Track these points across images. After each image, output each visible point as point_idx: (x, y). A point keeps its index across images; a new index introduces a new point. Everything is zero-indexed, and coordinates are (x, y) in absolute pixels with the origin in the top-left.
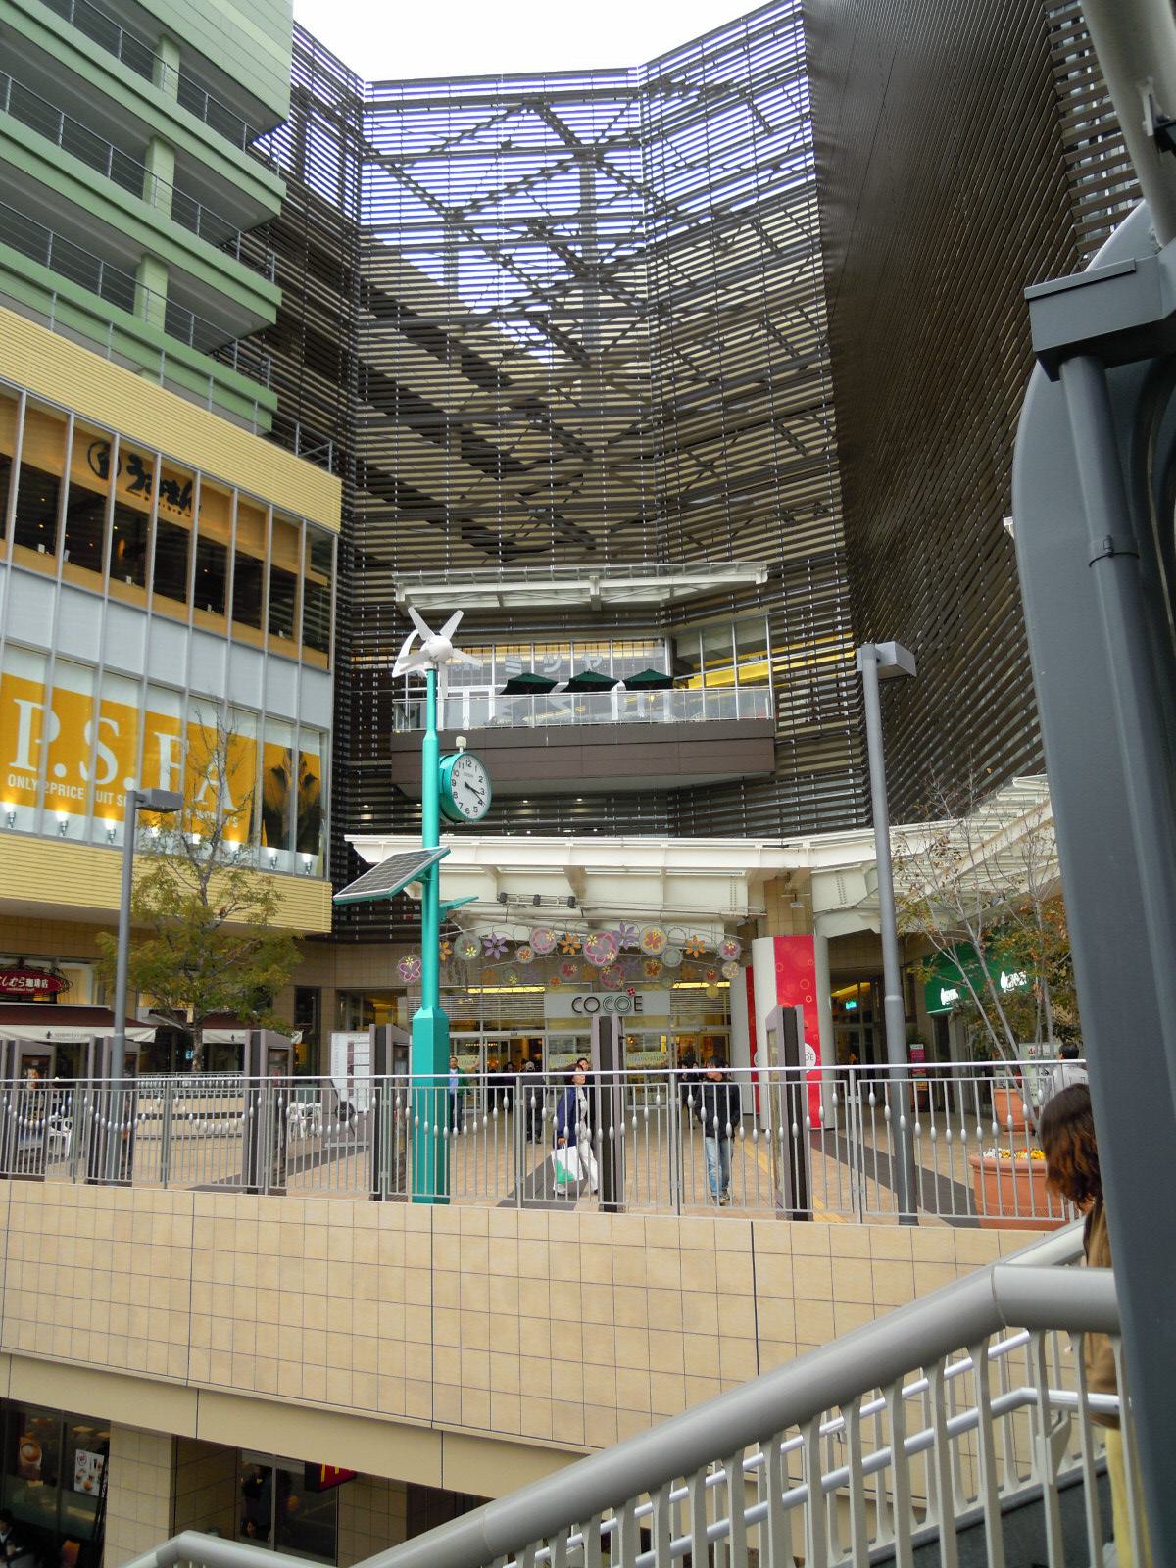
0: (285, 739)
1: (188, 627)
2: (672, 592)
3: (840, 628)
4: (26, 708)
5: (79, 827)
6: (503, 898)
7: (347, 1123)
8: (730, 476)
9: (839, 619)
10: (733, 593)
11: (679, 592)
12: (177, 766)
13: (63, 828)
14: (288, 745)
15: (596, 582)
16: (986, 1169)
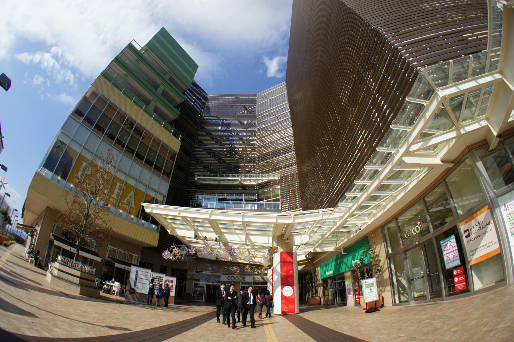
1: (122, 153)
5: (125, 214)
6: (196, 236)
7: (51, 321)
13: (132, 219)
14: (154, 196)
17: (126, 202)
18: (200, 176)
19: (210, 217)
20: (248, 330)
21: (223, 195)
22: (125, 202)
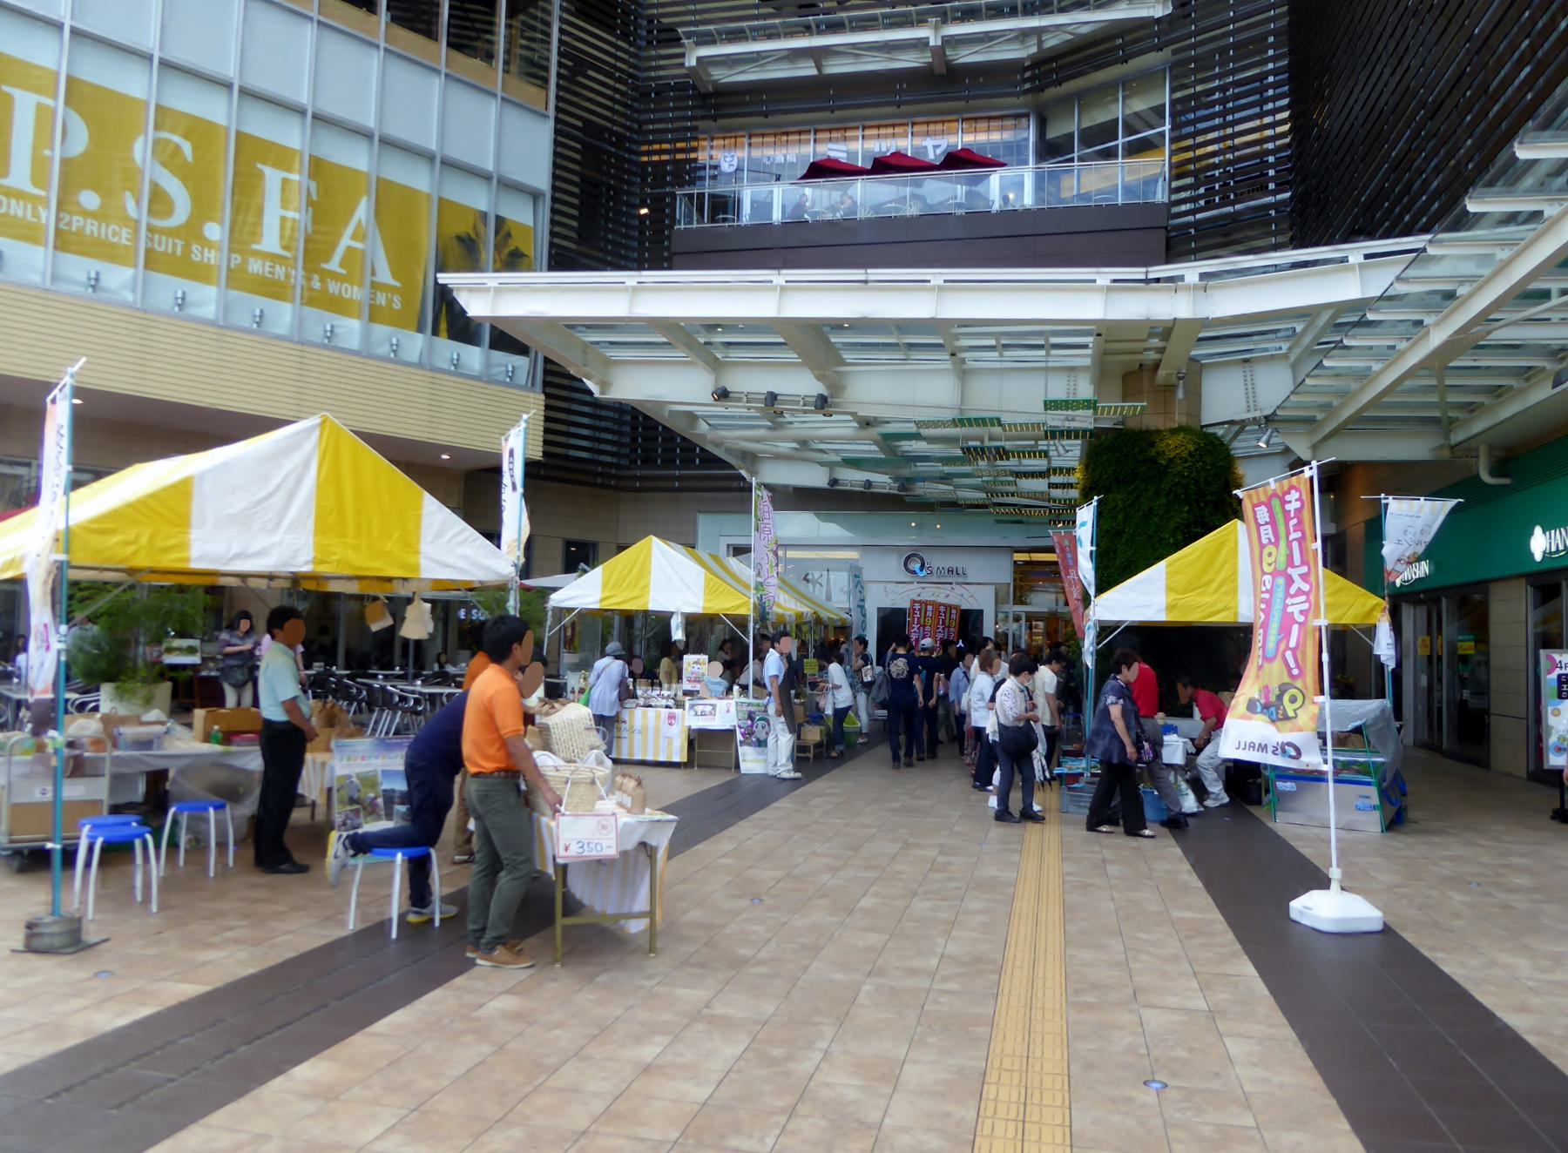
0: (478, 198)
2: (1040, 43)
3: (1271, 79)
4: (25, 104)
6: (723, 395)
8: (1199, 216)
9: (1271, 66)
10: (1121, 34)
11: (1051, 42)
12: (291, 214)
15: (936, 29)
16: (499, 181)
17: (342, 265)
18: (707, 39)
19: (779, 312)
20: (956, 828)
21: (845, 139)
22: (334, 265)
